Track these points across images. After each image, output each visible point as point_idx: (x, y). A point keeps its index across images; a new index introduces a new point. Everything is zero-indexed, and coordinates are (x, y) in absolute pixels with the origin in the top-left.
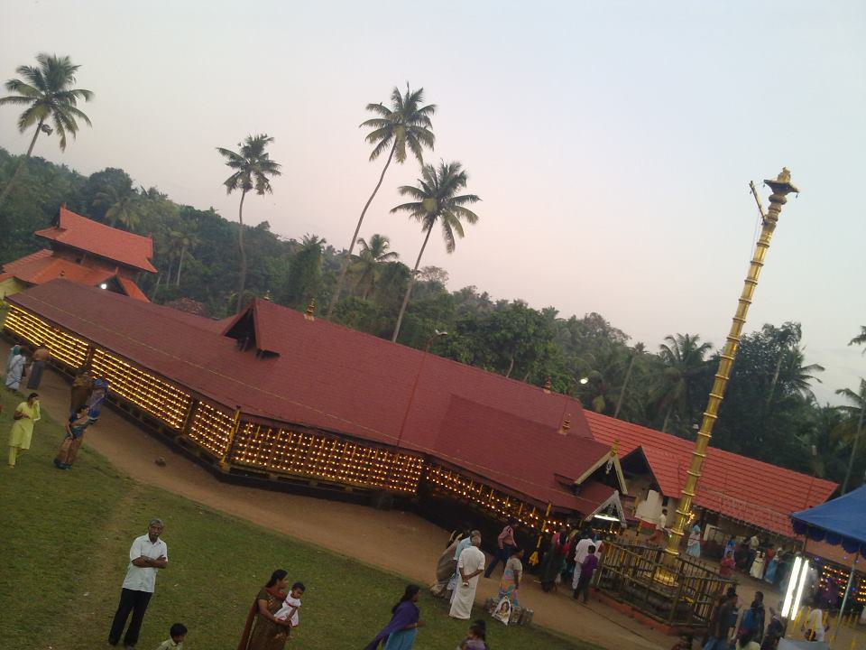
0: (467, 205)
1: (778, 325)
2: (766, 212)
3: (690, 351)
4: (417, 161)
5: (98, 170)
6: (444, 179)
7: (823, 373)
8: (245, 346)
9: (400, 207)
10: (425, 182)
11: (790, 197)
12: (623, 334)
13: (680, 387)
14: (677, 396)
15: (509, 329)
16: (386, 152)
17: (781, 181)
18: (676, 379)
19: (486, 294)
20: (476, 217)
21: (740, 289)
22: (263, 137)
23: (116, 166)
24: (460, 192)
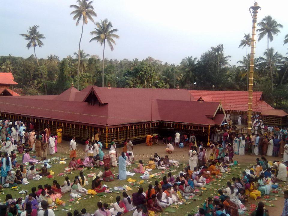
0: (114, 33)
1: (216, 47)
4: (92, 22)
6: (103, 26)
8: (93, 103)
9: (92, 40)
10: (98, 29)
11: (259, 10)
12: (160, 61)
13: (191, 74)
14: (191, 77)
15: (142, 71)
16: (81, 21)
17: (255, 6)
18: (189, 72)
19: (111, 59)
20: (119, 36)
22: (35, 26)
24: (111, 29)
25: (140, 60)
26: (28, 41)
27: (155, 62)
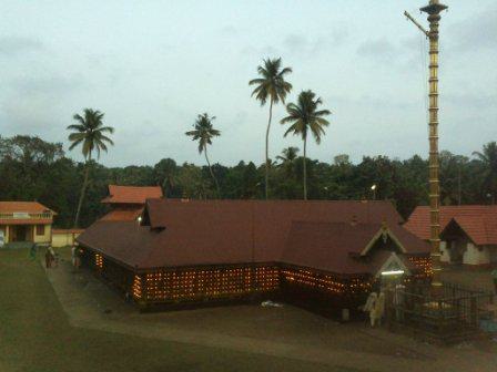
0: (324, 117)
2: (429, 29)
3: (416, 159)
5: (140, 163)
7: (315, 144)
11: (442, 13)
21: (426, 103)
23: (166, 157)
25: (391, 158)
26: (197, 142)
27: (454, 159)
